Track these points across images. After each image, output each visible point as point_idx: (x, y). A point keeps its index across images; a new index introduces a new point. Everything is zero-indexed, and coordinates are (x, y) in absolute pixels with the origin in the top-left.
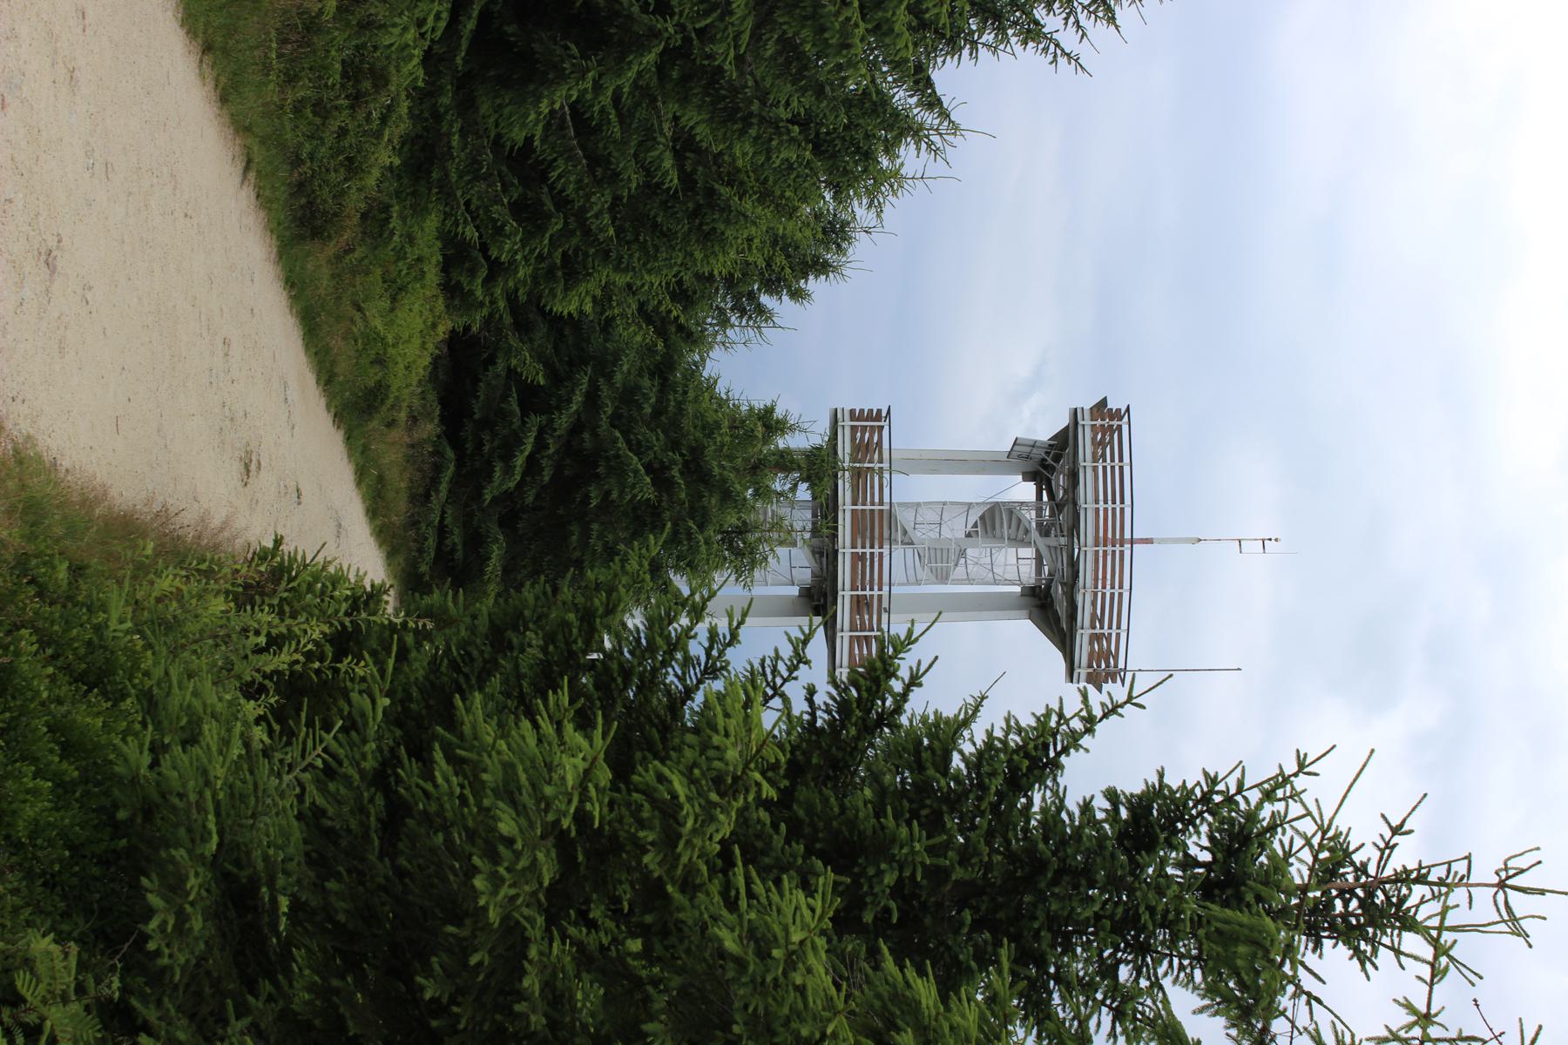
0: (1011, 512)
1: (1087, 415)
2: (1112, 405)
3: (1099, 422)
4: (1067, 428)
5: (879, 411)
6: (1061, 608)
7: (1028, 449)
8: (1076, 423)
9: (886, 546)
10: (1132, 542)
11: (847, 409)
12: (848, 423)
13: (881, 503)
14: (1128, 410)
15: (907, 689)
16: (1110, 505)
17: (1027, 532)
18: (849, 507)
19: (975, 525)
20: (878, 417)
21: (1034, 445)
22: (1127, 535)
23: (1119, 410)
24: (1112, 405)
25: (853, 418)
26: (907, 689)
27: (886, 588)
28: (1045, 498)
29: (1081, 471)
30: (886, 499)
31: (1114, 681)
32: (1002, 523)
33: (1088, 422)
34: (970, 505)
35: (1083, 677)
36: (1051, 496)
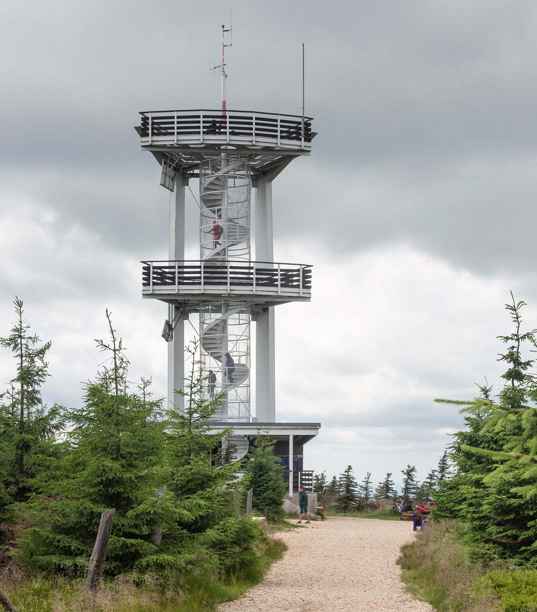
0: (206, 189)
1: (144, 139)
2: (139, 123)
3: (150, 132)
4: (154, 153)
5: (144, 268)
6: (268, 159)
7: (168, 178)
8: (151, 146)
9: (226, 264)
10: (224, 111)
11: (142, 287)
12: (151, 287)
13: (200, 267)
14: (142, 113)
15: (471, 404)
16: (254, 132)
17: (218, 179)
18: (202, 287)
19: (214, 212)
20: (147, 269)
21: (165, 174)
22: (221, 114)
23: (143, 119)
24: (139, 123)
25: (148, 284)
26: (471, 404)
27: (252, 265)
28: (197, 171)
29: (181, 292)
30: (198, 264)
31: (310, 125)
32: (211, 195)
33: (149, 139)
34: (202, 215)
35: (307, 144)
36: (196, 166)
